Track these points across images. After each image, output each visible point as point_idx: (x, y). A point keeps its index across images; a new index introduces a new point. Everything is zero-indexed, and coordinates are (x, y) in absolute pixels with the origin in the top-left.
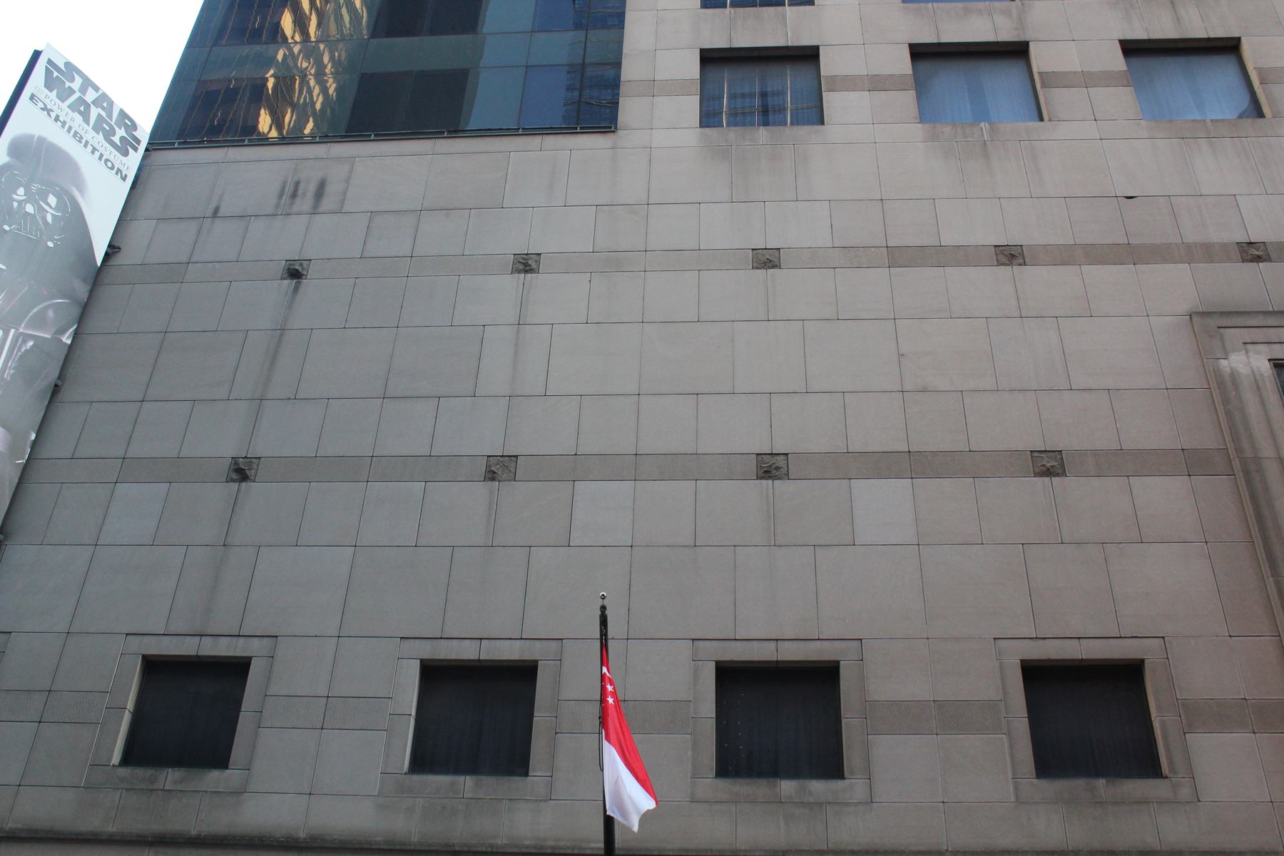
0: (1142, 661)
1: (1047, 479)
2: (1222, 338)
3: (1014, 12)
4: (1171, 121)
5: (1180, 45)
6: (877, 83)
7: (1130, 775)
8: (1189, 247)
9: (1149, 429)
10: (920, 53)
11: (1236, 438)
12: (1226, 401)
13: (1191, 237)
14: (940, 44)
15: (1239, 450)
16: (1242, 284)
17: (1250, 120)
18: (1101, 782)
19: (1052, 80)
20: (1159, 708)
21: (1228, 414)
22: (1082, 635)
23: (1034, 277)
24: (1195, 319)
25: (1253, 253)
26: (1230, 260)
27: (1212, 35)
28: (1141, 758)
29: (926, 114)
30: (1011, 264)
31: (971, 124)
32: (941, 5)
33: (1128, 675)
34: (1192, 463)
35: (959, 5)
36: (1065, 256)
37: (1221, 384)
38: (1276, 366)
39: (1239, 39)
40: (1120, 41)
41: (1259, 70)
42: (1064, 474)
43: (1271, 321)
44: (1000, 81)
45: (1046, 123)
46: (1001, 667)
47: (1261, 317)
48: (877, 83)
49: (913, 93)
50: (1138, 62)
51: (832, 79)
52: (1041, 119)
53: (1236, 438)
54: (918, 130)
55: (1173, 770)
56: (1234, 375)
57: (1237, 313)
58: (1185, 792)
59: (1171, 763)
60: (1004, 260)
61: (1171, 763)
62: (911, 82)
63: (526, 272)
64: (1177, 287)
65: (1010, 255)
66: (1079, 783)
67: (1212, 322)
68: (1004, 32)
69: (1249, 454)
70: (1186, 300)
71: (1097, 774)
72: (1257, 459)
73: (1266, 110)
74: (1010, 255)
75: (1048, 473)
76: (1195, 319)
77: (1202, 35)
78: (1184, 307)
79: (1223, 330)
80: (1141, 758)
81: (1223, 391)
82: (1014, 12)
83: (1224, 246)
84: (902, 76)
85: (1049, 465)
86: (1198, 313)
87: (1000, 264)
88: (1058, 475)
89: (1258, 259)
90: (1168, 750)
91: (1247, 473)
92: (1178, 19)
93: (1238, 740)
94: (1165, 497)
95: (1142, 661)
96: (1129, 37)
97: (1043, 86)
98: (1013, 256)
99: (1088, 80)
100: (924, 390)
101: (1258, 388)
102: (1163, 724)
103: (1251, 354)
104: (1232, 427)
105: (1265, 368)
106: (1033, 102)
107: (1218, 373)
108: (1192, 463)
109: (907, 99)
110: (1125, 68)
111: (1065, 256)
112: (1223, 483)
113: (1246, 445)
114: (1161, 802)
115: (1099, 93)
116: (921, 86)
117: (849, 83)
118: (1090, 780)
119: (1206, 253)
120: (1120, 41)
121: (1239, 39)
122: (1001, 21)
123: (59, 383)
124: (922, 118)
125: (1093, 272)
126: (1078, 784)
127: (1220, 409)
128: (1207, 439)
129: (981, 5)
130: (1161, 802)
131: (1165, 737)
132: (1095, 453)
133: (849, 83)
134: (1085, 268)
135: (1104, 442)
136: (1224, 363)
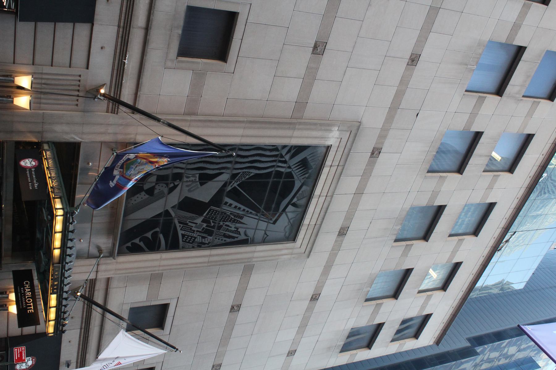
0: (226, 62)
1: (313, 46)
2: (347, 131)
3: (517, 96)
4: (84, 111)
7: (181, 44)
8: (388, 130)
9: (319, 93)
10: (520, 50)
11: (305, 124)
12: (321, 125)
13: (391, 132)
14: (520, 60)
15: (300, 124)
16: (365, 145)
17: (428, 168)
18: (180, 32)
19: (481, 101)
20: (206, 63)
21: (315, 124)
22: (242, 40)
23: (400, 67)
24: (358, 124)
25: (376, 152)
26: (376, 143)
28: (186, 50)
29: (492, 44)
30: (410, 59)
31: (477, 63)
32: (537, 66)
33: (222, 54)
34: (301, 104)
36: (404, 82)
37: (329, 125)
38: (328, 147)
42: (313, 53)
44: (491, 80)
46: (238, 3)
47: (349, 147)
48: (516, 27)
49: (504, 42)
51: (529, 7)
52: (466, 91)
53: (305, 124)
54: (486, 38)
55: (179, 62)
56: (330, 131)
58: (169, 64)
59: (182, 62)
60: (413, 57)
61: (182, 62)
64: (373, 121)
65: (414, 60)
66: (181, 22)
67: (355, 130)
68: (509, 89)
69: (297, 127)
71: (184, 30)
72: (294, 129)
73: (430, 174)
75: (315, 47)
76: (358, 124)
77: (470, 162)
78: (364, 121)
79: (349, 132)
80: (186, 50)
81: (325, 125)
82: (517, 96)
83: (383, 143)
84: (514, 39)
85: (319, 49)
86: (359, 127)
87: (412, 54)
88: (313, 51)
89: (373, 153)
90: (188, 62)
91: (290, 124)
92: (481, 156)
93: (187, 90)
94: (290, 91)
97: (480, 97)
98: (413, 61)
99: (473, 115)
101: (323, 138)
102: (198, 63)
104: (310, 124)
105: (328, 143)
106: (475, 90)
108: (301, 104)
109: (503, 40)
110: (471, 130)
111: (404, 82)
113: (301, 127)
115: (466, 117)
116: (504, 46)
117: (523, 14)
118: (182, 28)
122: (517, 89)
123: (228, 204)
124: (490, 42)
125: (393, 91)
126: (181, 22)
128: (309, 113)
131: (193, 62)
132: (317, 69)
133: (523, 14)
134: (396, 88)
135: (321, 74)
136: (336, 128)
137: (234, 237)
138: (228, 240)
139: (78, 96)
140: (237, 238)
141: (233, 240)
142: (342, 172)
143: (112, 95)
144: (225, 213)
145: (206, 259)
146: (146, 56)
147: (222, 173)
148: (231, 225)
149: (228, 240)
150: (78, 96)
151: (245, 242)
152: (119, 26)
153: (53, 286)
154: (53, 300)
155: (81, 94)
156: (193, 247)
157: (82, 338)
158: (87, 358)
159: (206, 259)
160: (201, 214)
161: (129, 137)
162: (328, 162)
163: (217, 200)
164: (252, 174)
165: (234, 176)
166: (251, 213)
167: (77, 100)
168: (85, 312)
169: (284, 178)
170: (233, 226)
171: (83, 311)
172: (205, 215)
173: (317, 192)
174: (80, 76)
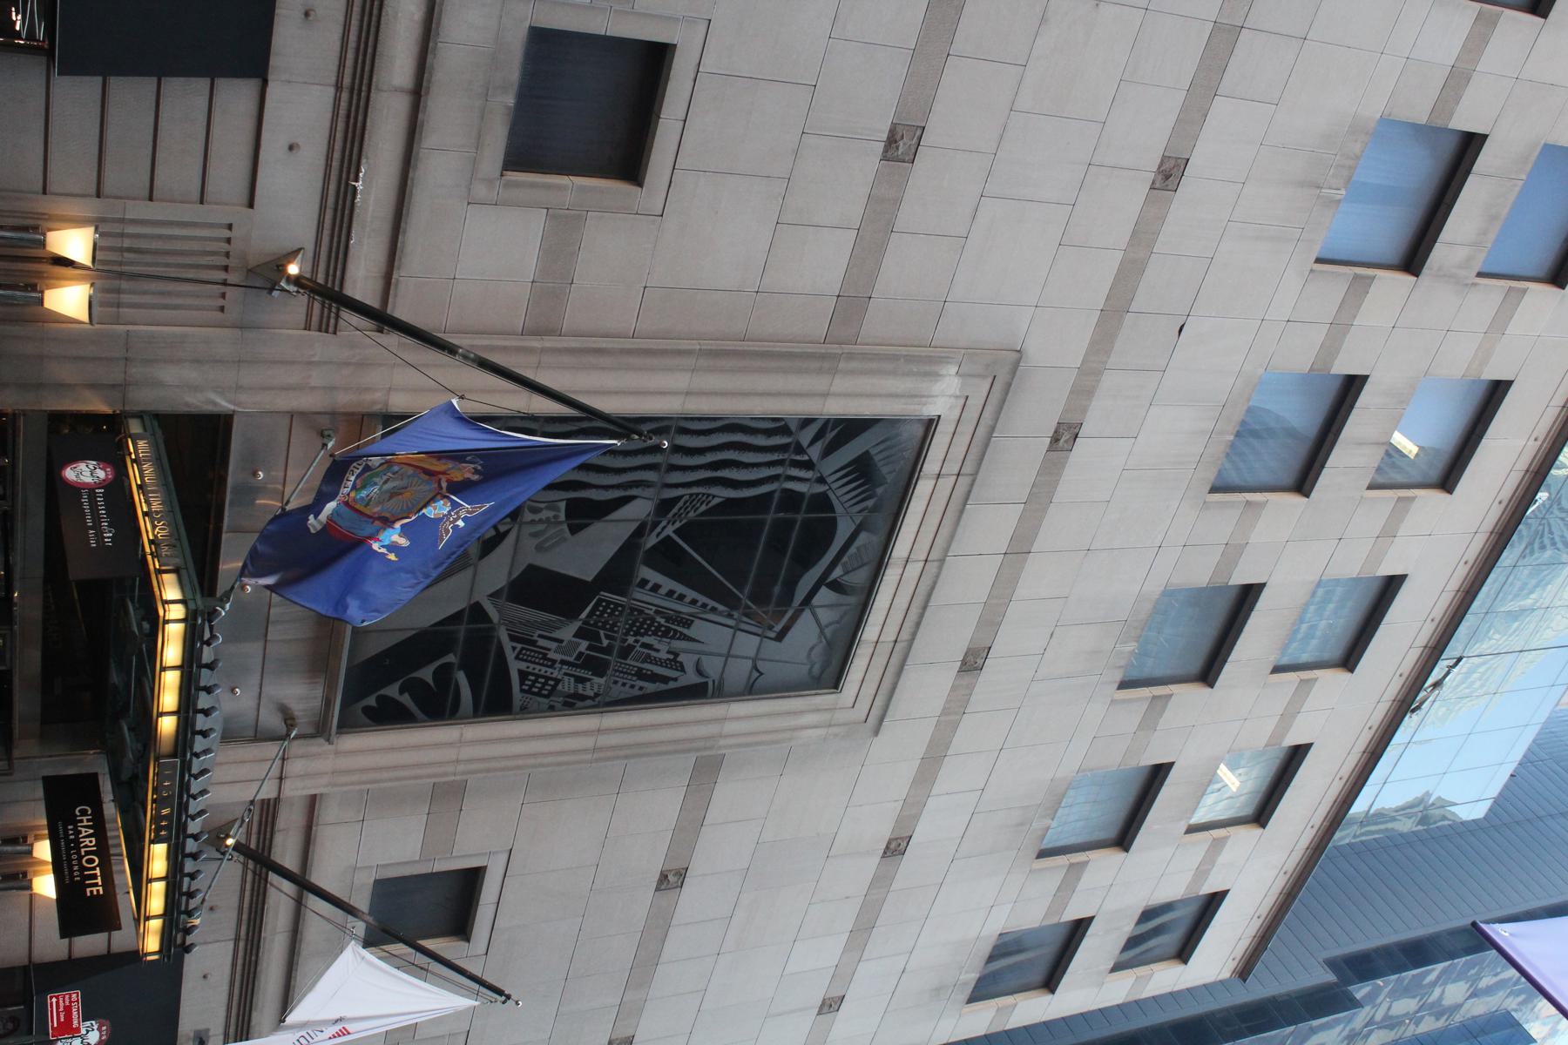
0: (640, 185)
1: (884, 137)
5: (1331, 436)
6: (1458, 79)
7: (513, 133)
8: (1098, 373)
9: (904, 270)
10: (1470, 144)
11: (865, 357)
12: (909, 359)
13: (1108, 380)
14: (1468, 172)
15: (851, 356)
16: (1034, 415)
18: (511, 101)
19: (1360, 288)
20: (582, 189)
21: (894, 358)
23: (1132, 195)
24: (1015, 355)
25: (1064, 436)
26: (1065, 411)
27: (1354, 412)
28: (529, 152)
29: (1390, 128)
30: (1159, 171)
32: (1517, 189)
35: (1505, 211)
36: (1143, 237)
37: (930, 360)
38: (931, 421)
39: (1307, 496)
40: (1484, 137)
41: (1262, 505)
42: (885, 158)
43: (982, 430)
44: (1387, 229)
45: (1310, 264)
48: (1458, 79)
49: (1423, 120)
50: (1333, 388)
52: (1319, 261)
53: (865, 357)
54: (1374, 109)
55: (508, 185)
56: (936, 376)
57: (1004, 401)
58: (481, 191)
59: (518, 185)
60: (1166, 166)
61: (518, 185)
62: (1439, 123)
63: (964, 662)
64: (1056, 348)
65: (1170, 174)
66: (514, 74)
67: (1004, 372)
68: (1440, 254)
70: (1036, 352)
72: (834, 372)
74: (1170, 174)
75: (892, 141)
76: (1015, 355)
80: (529, 152)
81: (921, 359)
83: (1084, 410)
85: (901, 145)
87: (1164, 158)
88: (886, 151)
89: (1055, 439)
91: (823, 357)
93: (530, 264)
94: (820, 265)
95: (640, 185)
96: (1260, 605)
97: (1356, 277)
98: (1167, 177)
99: (1339, 328)
100: (1043, 20)
103: (953, 400)
105: (930, 411)
107: (943, 360)
108: (852, 302)
111: (1143, 237)
112: (820, 328)
113: (854, 365)
114: (475, 162)
115: (1318, 335)
116: (1426, 133)
119: (1085, 388)
120: (1484, 137)
121: (1307, 496)
122: (1461, 253)
124: (1386, 122)
126: (513, 73)
127: (904, 351)
128: (877, 324)
129: (1492, 236)
130: (475, 162)
131: (548, 187)
132: (897, 202)
134: (1120, 255)
135: (908, 215)
136: (953, 369)
137: (665, 680)
138: (651, 687)
139: (225, 283)
140: (675, 679)
141: (662, 687)
142: (969, 492)
143: (321, 280)
144: (641, 612)
145: (589, 742)
146: (427, 93)
147: (633, 498)
148: (657, 646)
149: (651, 687)
150: (225, 283)
151: (697, 693)
152: (338, 87)
153: (157, 818)
154: (158, 858)
155: (232, 278)
156: (552, 708)
157: (239, 968)
158: (253, 1023)
159: (589, 742)
160: (572, 615)
161: (368, 397)
162: (931, 465)
163: (617, 574)
164: (716, 501)
165: (664, 507)
166: (714, 610)
167: (223, 296)
168: (247, 894)
169: (807, 512)
170: (662, 648)
171: (243, 890)
172: (583, 616)
173: (900, 549)
174: (230, 227)
